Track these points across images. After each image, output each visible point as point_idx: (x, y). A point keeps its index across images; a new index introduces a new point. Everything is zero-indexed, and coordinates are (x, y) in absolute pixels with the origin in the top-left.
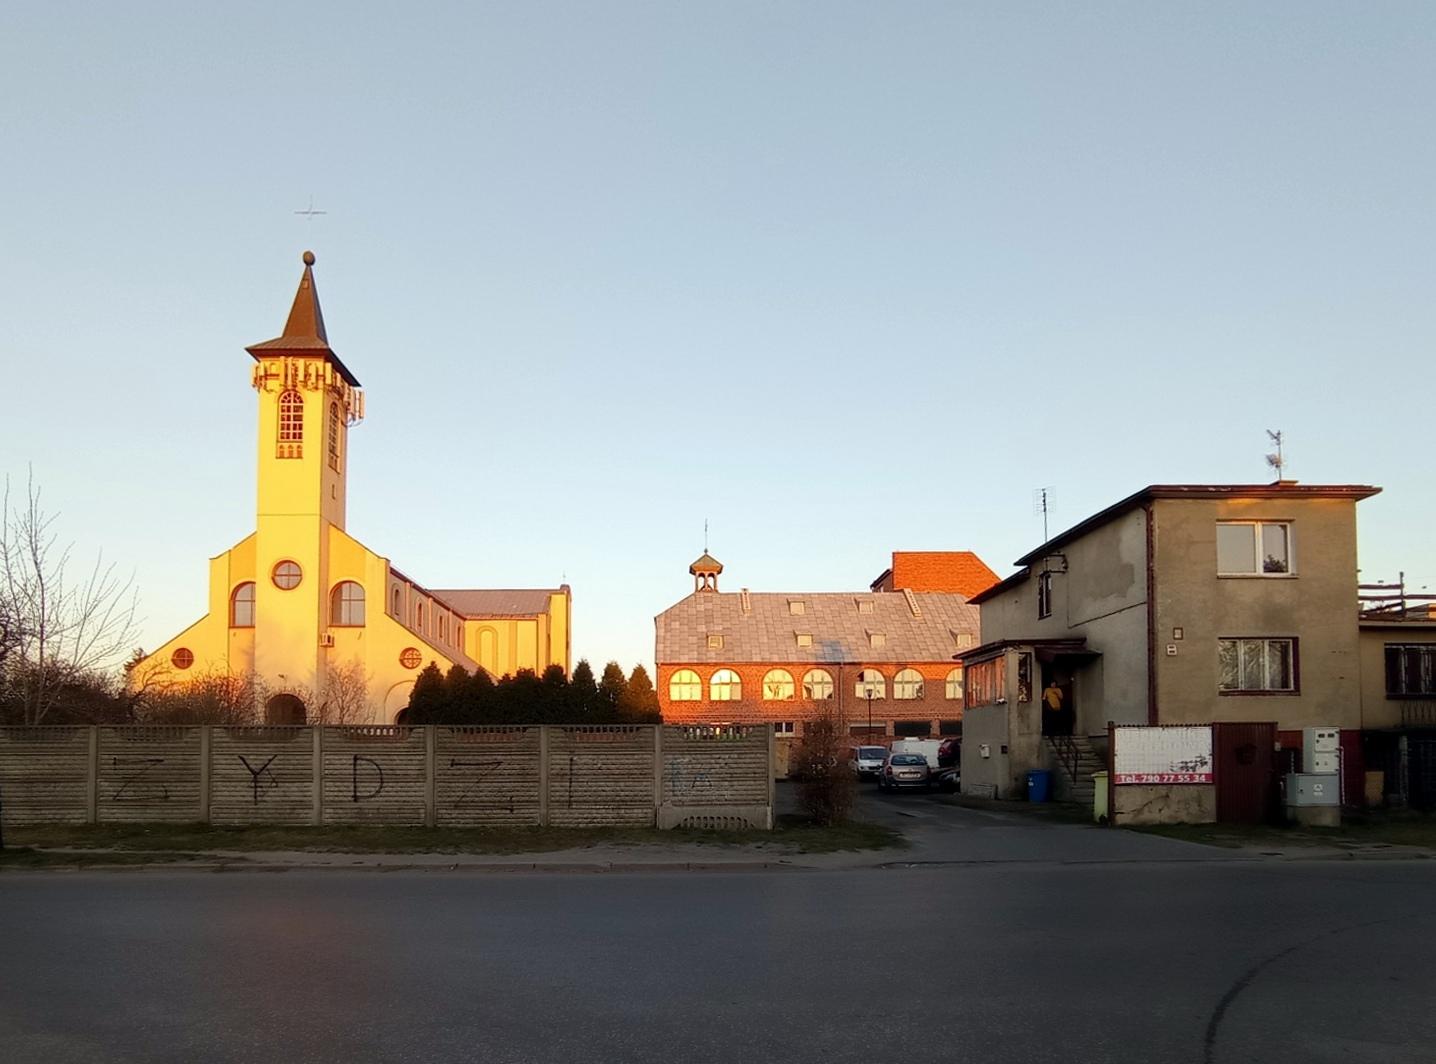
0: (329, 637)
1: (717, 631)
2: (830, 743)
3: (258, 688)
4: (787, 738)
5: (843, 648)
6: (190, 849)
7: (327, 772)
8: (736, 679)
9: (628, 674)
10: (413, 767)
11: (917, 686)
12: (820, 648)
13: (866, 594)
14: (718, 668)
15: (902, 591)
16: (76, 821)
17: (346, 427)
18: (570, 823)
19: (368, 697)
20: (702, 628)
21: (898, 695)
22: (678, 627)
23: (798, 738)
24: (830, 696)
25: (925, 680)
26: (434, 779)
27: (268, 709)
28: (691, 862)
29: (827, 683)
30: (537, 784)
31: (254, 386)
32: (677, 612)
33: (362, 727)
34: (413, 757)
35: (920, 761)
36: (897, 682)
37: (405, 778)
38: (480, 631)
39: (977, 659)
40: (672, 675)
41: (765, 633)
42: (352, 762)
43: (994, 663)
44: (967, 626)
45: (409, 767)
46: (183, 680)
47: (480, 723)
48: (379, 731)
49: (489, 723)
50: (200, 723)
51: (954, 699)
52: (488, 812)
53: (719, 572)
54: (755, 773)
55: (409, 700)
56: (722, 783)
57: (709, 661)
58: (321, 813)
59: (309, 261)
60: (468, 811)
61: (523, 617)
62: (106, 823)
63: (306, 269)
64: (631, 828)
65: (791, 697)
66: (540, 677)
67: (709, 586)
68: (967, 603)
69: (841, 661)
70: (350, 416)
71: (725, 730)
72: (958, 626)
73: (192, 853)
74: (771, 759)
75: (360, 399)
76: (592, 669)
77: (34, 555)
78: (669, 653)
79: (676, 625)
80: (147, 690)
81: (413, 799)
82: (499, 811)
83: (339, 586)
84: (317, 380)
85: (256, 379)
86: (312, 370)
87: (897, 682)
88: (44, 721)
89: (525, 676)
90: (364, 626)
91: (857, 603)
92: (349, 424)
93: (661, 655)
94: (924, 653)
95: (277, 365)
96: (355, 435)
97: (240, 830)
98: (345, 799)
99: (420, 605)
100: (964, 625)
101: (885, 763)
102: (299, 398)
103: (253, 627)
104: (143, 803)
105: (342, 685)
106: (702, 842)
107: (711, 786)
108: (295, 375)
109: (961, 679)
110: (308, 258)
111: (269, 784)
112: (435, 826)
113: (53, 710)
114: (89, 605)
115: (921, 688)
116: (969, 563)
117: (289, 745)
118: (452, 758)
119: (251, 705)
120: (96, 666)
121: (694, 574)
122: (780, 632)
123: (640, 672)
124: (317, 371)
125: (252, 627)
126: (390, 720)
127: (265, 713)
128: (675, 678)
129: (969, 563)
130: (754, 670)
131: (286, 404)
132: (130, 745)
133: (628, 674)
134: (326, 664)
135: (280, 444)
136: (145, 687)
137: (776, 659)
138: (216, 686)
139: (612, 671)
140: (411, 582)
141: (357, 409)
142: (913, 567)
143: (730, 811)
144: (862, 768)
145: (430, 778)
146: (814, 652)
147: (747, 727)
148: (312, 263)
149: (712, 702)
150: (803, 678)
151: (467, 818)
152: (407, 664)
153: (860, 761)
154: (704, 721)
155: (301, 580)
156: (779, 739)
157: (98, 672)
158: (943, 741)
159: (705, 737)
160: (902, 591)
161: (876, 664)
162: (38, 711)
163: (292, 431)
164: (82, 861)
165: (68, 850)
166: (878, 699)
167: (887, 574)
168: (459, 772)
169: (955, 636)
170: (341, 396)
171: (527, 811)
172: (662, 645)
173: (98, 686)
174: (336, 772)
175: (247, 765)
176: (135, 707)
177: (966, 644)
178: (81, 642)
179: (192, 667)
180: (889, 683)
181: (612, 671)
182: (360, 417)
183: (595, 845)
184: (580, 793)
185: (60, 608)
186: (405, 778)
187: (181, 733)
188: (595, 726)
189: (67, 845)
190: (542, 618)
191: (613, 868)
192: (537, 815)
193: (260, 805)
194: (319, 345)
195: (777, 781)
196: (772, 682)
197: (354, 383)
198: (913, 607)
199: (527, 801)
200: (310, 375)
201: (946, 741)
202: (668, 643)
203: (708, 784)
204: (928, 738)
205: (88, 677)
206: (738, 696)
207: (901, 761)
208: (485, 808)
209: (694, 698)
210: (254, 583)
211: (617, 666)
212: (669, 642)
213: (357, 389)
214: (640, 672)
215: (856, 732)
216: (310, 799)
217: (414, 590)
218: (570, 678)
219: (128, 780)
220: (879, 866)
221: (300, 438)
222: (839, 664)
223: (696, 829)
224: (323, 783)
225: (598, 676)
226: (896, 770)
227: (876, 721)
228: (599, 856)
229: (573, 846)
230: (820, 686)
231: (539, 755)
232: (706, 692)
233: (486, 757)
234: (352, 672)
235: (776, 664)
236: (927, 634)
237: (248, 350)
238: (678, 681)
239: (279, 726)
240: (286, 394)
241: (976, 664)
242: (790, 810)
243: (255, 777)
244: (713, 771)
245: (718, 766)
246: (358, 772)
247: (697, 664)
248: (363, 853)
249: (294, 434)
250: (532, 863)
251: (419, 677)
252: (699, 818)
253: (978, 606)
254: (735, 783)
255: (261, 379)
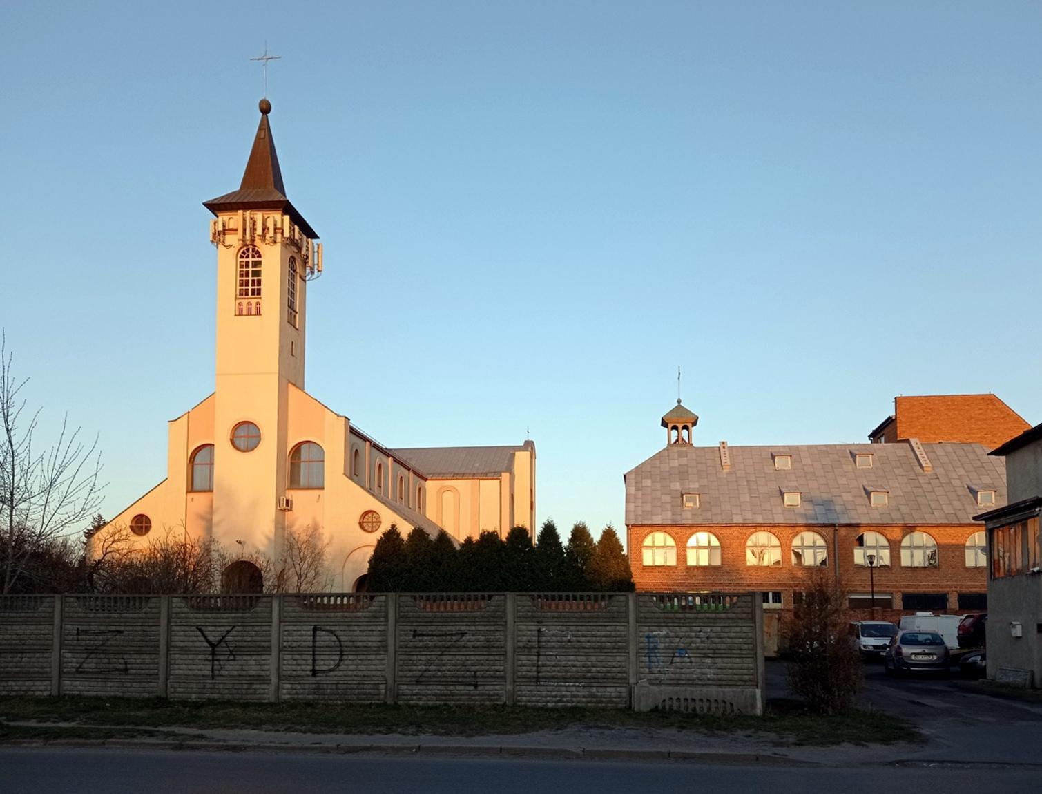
0: (287, 501)
1: (694, 489)
2: (827, 617)
3: (215, 555)
4: (775, 610)
5: (837, 508)
6: (149, 725)
7: (285, 644)
8: (715, 542)
9: (596, 536)
10: (374, 639)
11: (929, 552)
12: (811, 508)
13: (864, 445)
14: (694, 529)
15: (907, 441)
16: (41, 693)
17: (305, 281)
18: (538, 702)
19: (326, 563)
20: (677, 486)
21: (905, 561)
22: (650, 485)
23: (788, 610)
24: (823, 562)
25: (938, 545)
26: (395, 652)
27: (224, 577)
28: (672, 750)
29: (820, 547)
30: (502, 658)
31: (212, 242)
32: (649, 469)
33: (322, 596)
34: (374, 628)
35: (935, 640)
36: (906, 548)
37: (366, 651)
38: (441, 491)
39: (1004, 520)
40: (688, 538)
41: (746, 490)
42: (311, 633)
43: (1025, 526)
44: (990, 481)
45: (370, 639)
46: (141, 548)
47: (442, 590)
48: (339, 599)
49: (451, 590)
50: (158, 593)
51: (976, 568)
52: (451, 688)
53: (694, 424)
54: (741, 649)
55: (367, 566)
56: (704, 660)
57: (684, 522)
58: (278, 689)
59: (265, 109)
60: (430, 687)
61: (485, 475)
62: (69, 696)
63: (262, 118)
64: (604, 709)
65: (778, 562)
66: (504, 540)
67: (683, 440)
68: (989, 454)
69: (836, 522)
70: (308, 270)
71: (705, 598)
72: (979, 482)
73: (151, 728)
74: (758, 633)
75: (318, 252)
76: (559, 531)
77: (6, 421)
78: (640, 513)
79: (648, 482)
80: (107, 558)
81: (374, 673)
82: (462, 687)
83: (297, 448)
84: (275, 233)
85: (214, 234)
86: (270, 224)
87: (906, 548)
88: (12, 591)
89: (489, 539)
90: (323, 488)
91: (853, 455)
92: (307, 278)
93: (632, 516)
94: (937, 513)
95: (235, 219)
96: (314, 290)
97: (198, 705)
98: (303, 673)
99: (380, 465)
100: (986, 480)
101: (893, 641)
102: (258, 252)
103: (211, 491)
104: (103, 675)
105: (300, 549)
106: (683, 728)
107: (691, 662)
108: (253, 230)
109: (984, 544)
110: (265, 107)
111: (226, 657)
112: (396, 703)
113: (21, 578)
114: (55, 472)
115: (933, 554)
116: (990, 407)
117: (247, 615)
118: (413, 628)
119: (208, 574)
120: (58, 534)
121: (667, 427)
122: (763, 489)
123: (609, 534)
124: (275, 225)
125: (211, 491)
126: (348, 589)
127: (222, 581)
128: (648, 541)
129: (990, 407)
130: (736, 532)
131: (245, 260)
132: (92, 615)
133: (596, 536)
134: (284, 529)
135: (238, 301)
136: (104, 556)
137: (760, 520)
138: (174, 554)
139: (580, 533)
140: (370, 442)
141: (316, 263)
142: (920, 413)
143: (714, 691)
144: (865, 646)
145: (391, 649)
146: (803, 512)
147: (731, 596)
148: (269, 112)
149: (689, 568)
150: (791, 542)
151: (428, 695)
152: (366, 528)
153: (863, 639)
154: (679, 589)
155: (260, 440)
156: (766, 611)
157: (60, 540)
158: (963, 617)
159: (683, 608)
160: (907, 441)
161: (877, 525)
162: (7, 580)
163: (250, 288)
164: (48, 735)
165: (33, 723)
166: (882, 566)
167: (889, 422)
168: (421, 644)
169: (974, 493)
170: (300, 249)
171: (492, 687)
172: (633, 505)
173: (59, 556)
174: (295, 644)
175: (205, 637)
176: (95, 576)
177: (991, 502)
178: (47, 509)
179: (150, 533)
180: (895, 547)
181: (580, 533)
182: (319, 271)
183: (566, 727)
184: (548, 668)
185: (29, 474)
186: (366, 651)
187: (141, 603)
188: (564, 594)
189: (33, 718)
190: (506, 476)
191: (586, 754)
192: (501, 691)
193: (218, 680)
194: (277, 197)
195: (767, 659)
196: (756, 546)
197: (311, 234)
198: (921, 460)
199: (492, 677)
200: (268, 229)
201: (967, 617)
202: (639, 502)
203: (688, 660)
204: (945, 614)
205: (52, 545)
206: (717, 562)
207: (911, 640)
208: (448, 683)
209: (668, 564)
210: (213, 445)
211: (584, 528)
212: (640, 501)
213: (315, 241)
214: (609, 534)
215: (857, 604)
216: (268, 673)
217: (374, 450)
218: (535, 541)
219: (90, 651)
220: (892, 764)
221: (259, 293)
222: (833, 525)
223: (675, 712)
224: (281, 656)
225: (565, 538)
226: (906, 650)
227: (880, 593)
228: (570, 740)
229: (541, 728)
230: (812, 551)
231: (505, 625)
232: (682, 557)
233: (449, 628)
234: (311, 536)
235: (761, 525)
236: (939, 491)
237: (205, 204)
238: (651, 545)
239: (238, 595)
240: (245, 249)
241: (1002, 526)
242: (780, 694)
243: (213, 649)
244: (693, 645)
245: (698, 640)
246: (317, 644)
247: (671, 525)
248: (322, 732)
249: (253, 290)
250: (499, 746)
251: (379, 541)
252: (678, 699)
253: (1003, 458)
254: (720, 660)
255: (219, 235)
